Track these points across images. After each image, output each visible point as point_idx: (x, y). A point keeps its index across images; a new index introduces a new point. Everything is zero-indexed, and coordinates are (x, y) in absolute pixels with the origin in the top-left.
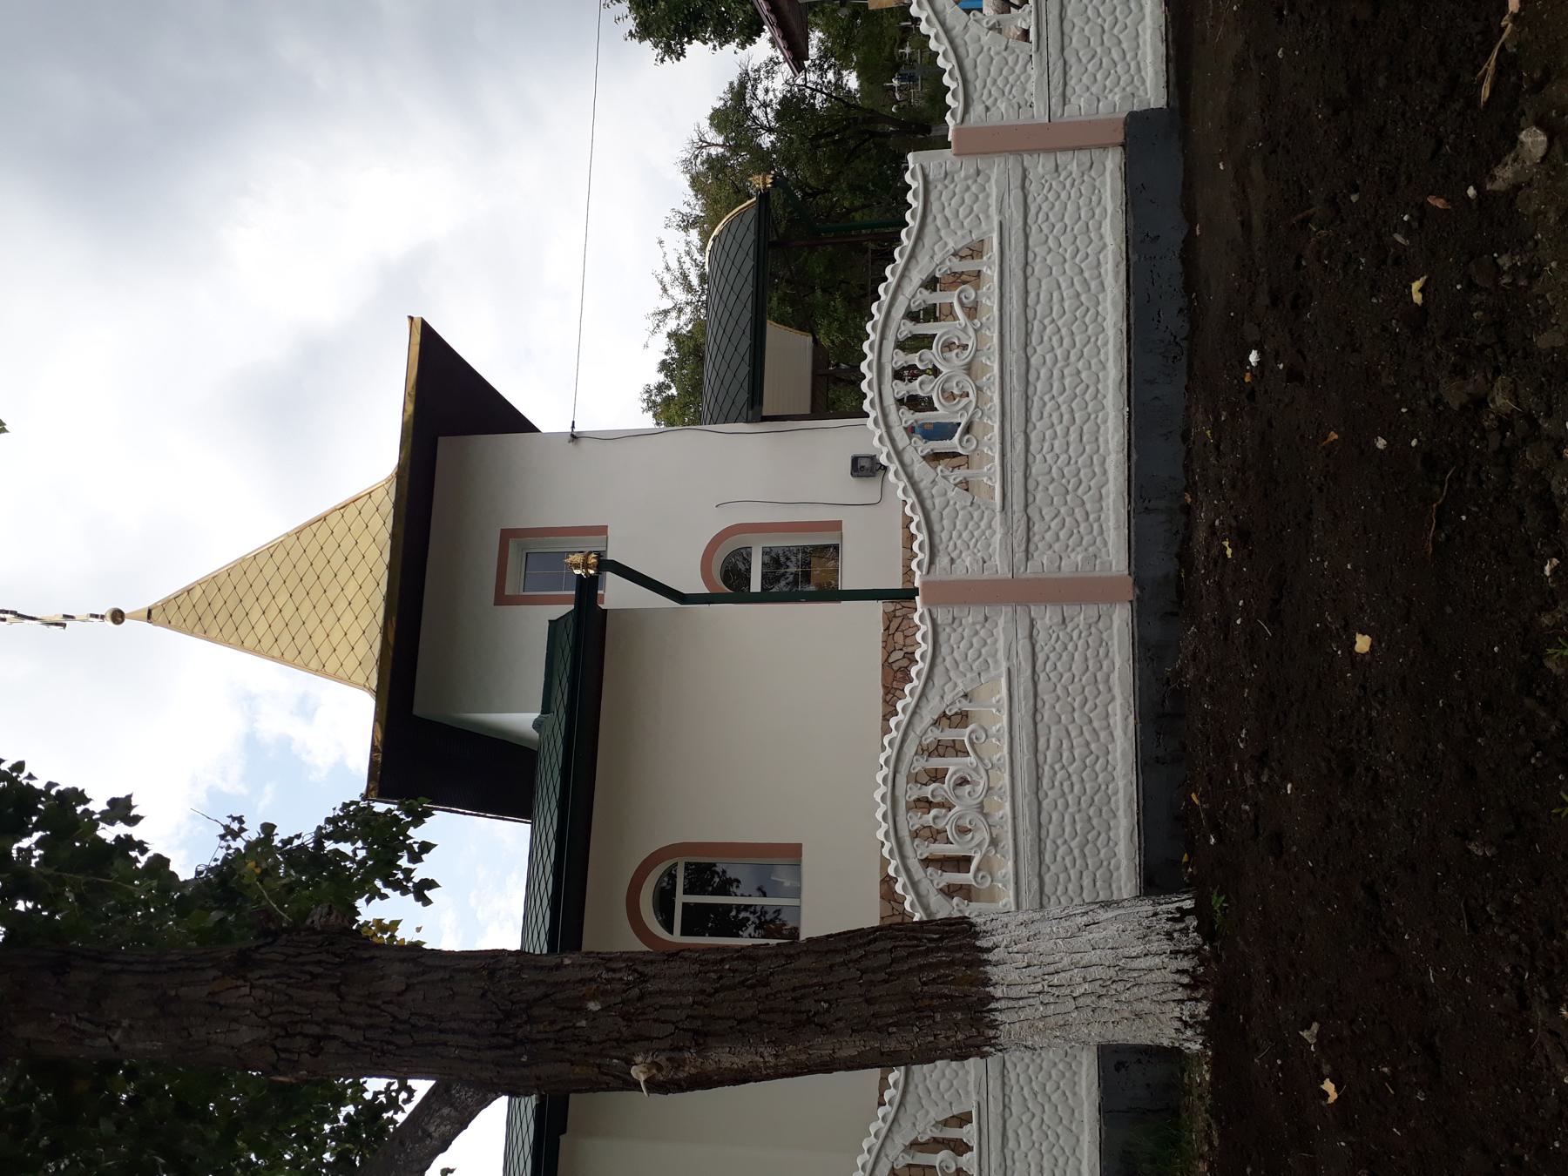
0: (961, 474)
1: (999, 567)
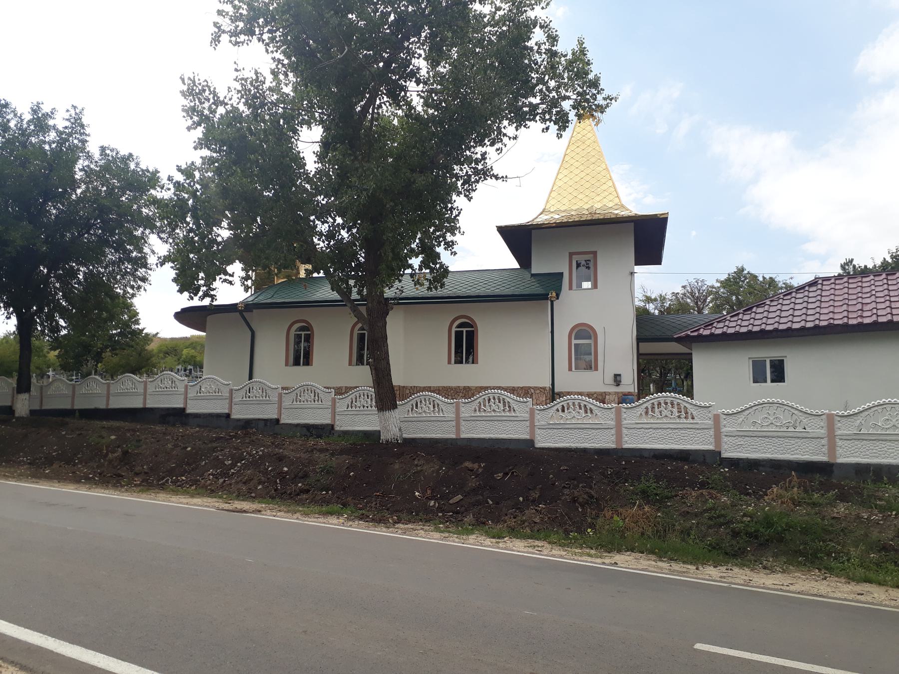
0: (643, 414)
1: (462, 415)
